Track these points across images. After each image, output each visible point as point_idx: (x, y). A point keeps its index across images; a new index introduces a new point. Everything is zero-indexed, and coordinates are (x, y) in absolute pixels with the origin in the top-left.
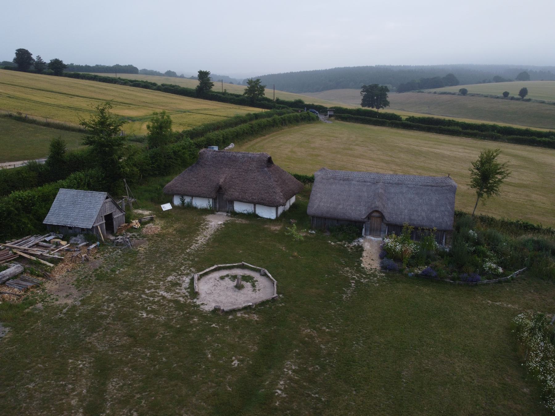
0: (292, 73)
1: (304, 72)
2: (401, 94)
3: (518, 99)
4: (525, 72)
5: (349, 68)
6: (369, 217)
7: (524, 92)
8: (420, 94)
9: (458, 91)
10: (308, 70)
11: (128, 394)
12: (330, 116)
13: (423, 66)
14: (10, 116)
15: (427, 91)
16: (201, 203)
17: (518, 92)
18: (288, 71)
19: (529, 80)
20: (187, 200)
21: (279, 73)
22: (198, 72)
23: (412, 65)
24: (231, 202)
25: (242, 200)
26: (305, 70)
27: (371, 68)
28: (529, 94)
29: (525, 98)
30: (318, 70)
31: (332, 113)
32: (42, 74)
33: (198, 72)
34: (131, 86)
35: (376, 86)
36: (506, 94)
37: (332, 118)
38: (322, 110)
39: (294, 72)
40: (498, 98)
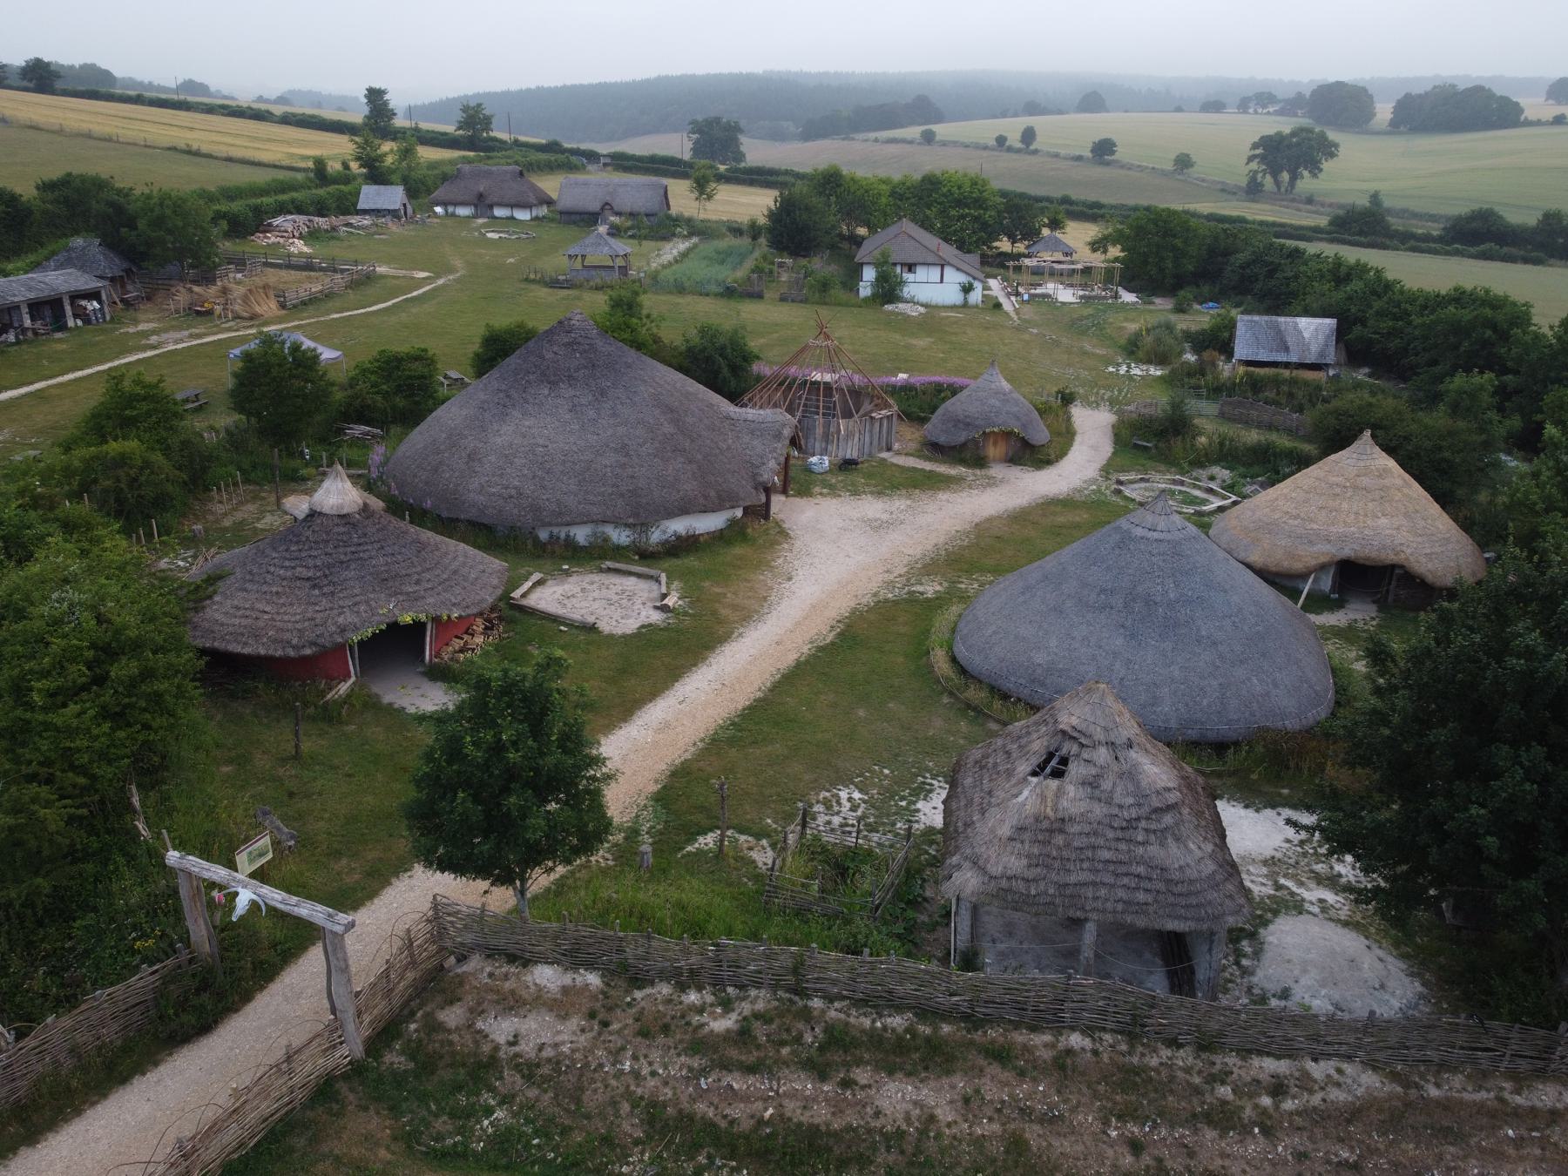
0: (540, 90)
1: (574, 87)
2: (809, 144)
3: (1018, 151)
4: (1095, 93)
5: (582, 86)
6: (602, 209)
7: (1029, 135)
8: (846, 142)
9: (918, 136)
10: (586, 81)
11: (744, 999)
12: (605, 165)
13: (826, 74)
14: (174, 149)
15: (861, 136)
16: (463, 211)
17: (1018, 136)
18: (531, 83)
19: (1108, 111)
20: (450, 209)
21: (504, 88)
22: (375, 95)
23: (857, 71)
24: (491, 207)
25: (501, 205)
26: (576, 81)
27: (750, 78)
28: (1039, 138)
29: (1032, 147)
30: (613, 81)
31: (608, 160)
32: (53, 93)
33: (375, 95)
34: (223, 115)
35: (717, 120)
36: (1001, 140)
37: (609, 168)
38: (592, 156)
39: (546, 86)
40: (986, 148)
